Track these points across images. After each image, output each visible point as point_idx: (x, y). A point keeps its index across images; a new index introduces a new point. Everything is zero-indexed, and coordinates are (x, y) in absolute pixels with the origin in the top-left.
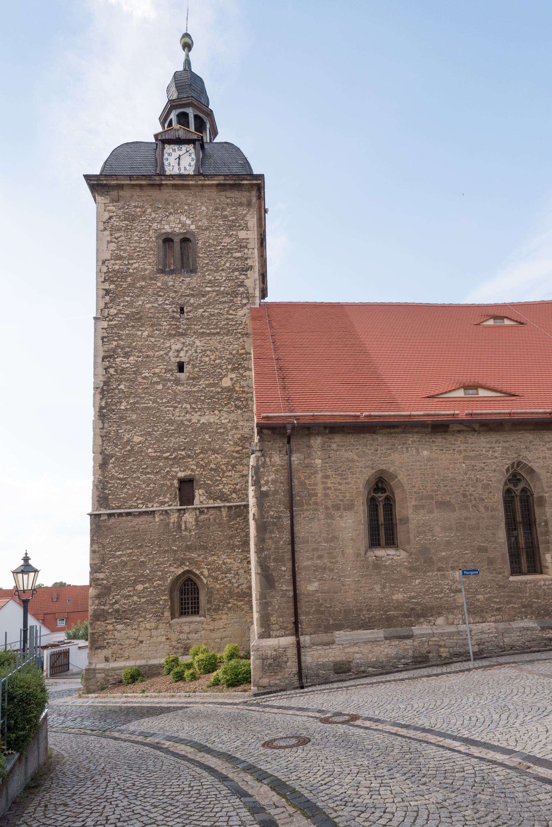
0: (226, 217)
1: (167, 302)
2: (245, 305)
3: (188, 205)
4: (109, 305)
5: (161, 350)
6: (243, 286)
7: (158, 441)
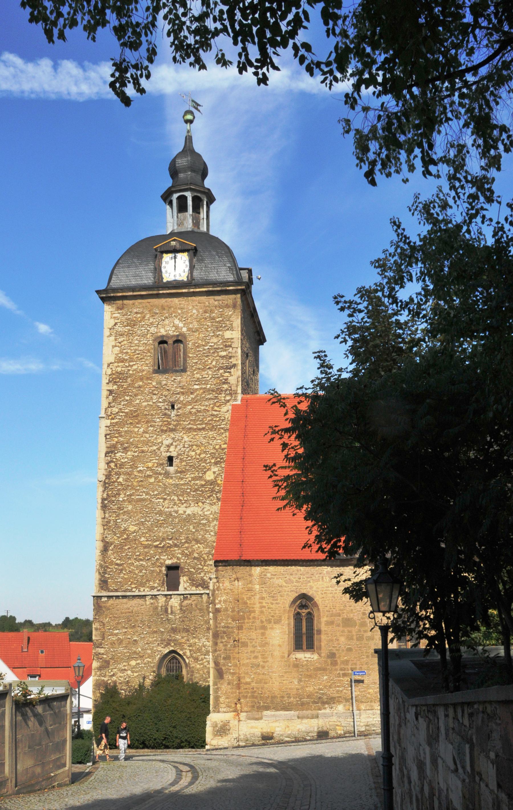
0: (213, 318)
1: (160, 400)
2: (228, 401)
3: (182, 309)
4: (112, 405)
5: (154, 445)
6: (227, 383)
7: (150, 530)
